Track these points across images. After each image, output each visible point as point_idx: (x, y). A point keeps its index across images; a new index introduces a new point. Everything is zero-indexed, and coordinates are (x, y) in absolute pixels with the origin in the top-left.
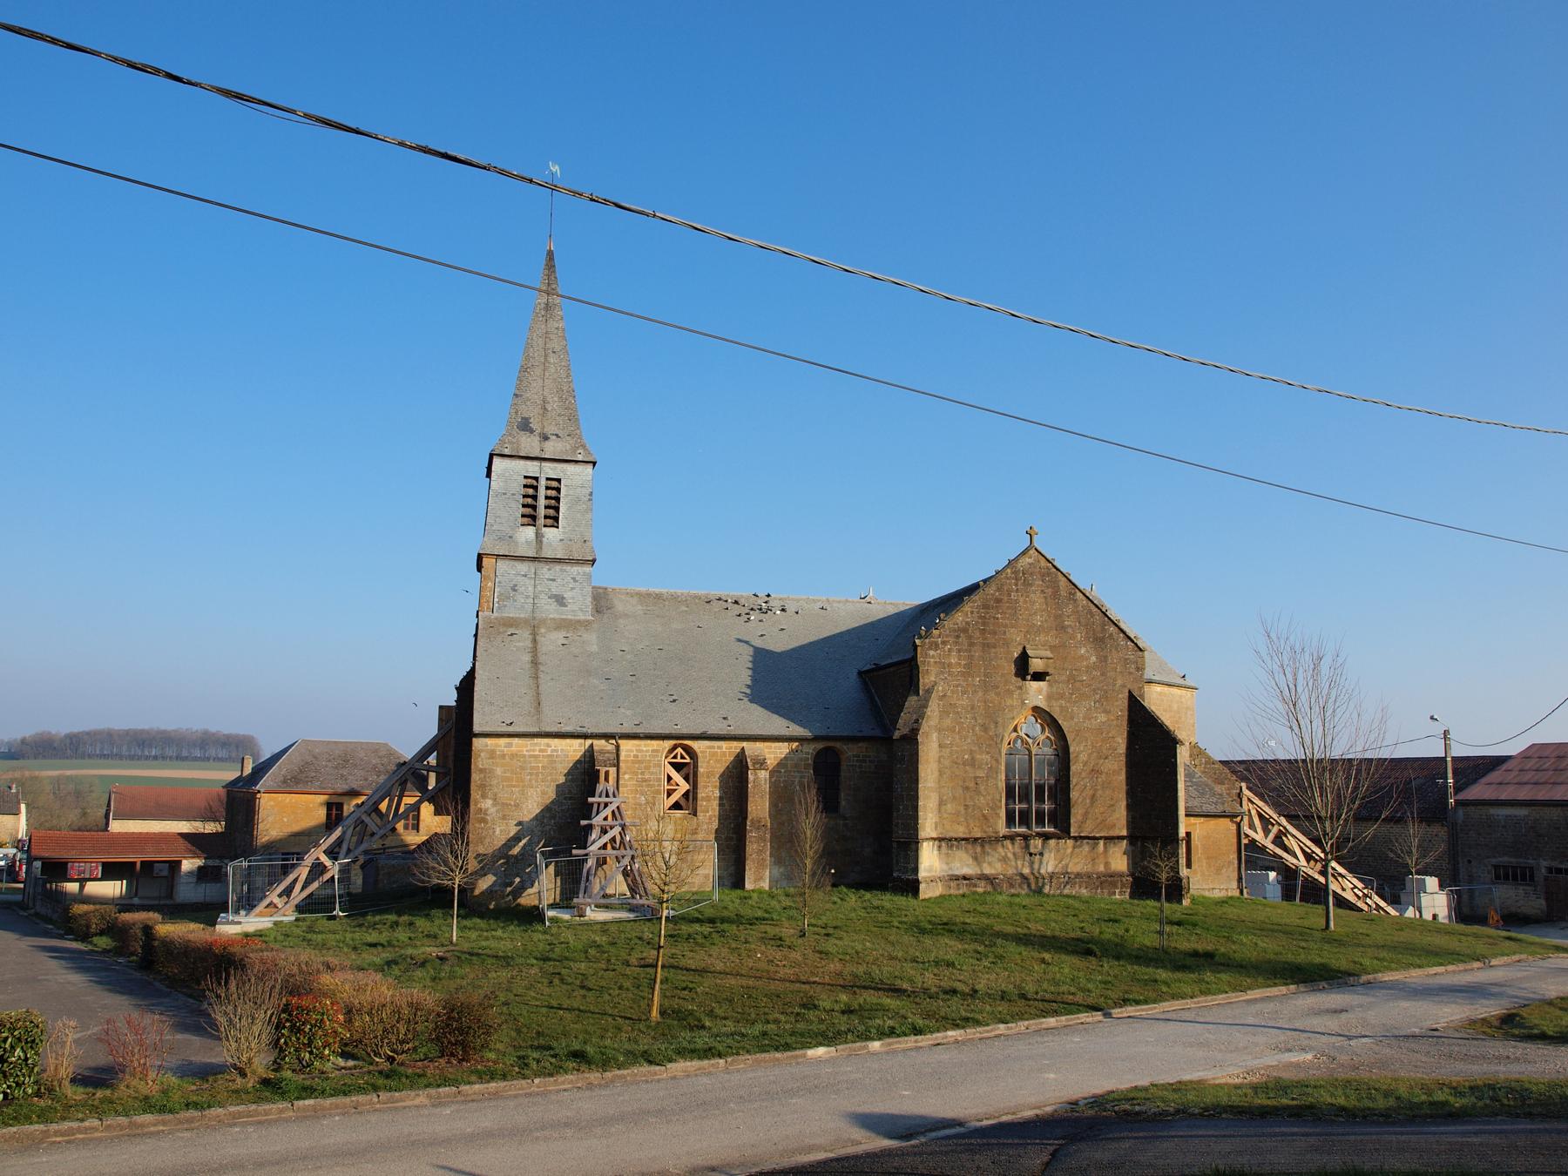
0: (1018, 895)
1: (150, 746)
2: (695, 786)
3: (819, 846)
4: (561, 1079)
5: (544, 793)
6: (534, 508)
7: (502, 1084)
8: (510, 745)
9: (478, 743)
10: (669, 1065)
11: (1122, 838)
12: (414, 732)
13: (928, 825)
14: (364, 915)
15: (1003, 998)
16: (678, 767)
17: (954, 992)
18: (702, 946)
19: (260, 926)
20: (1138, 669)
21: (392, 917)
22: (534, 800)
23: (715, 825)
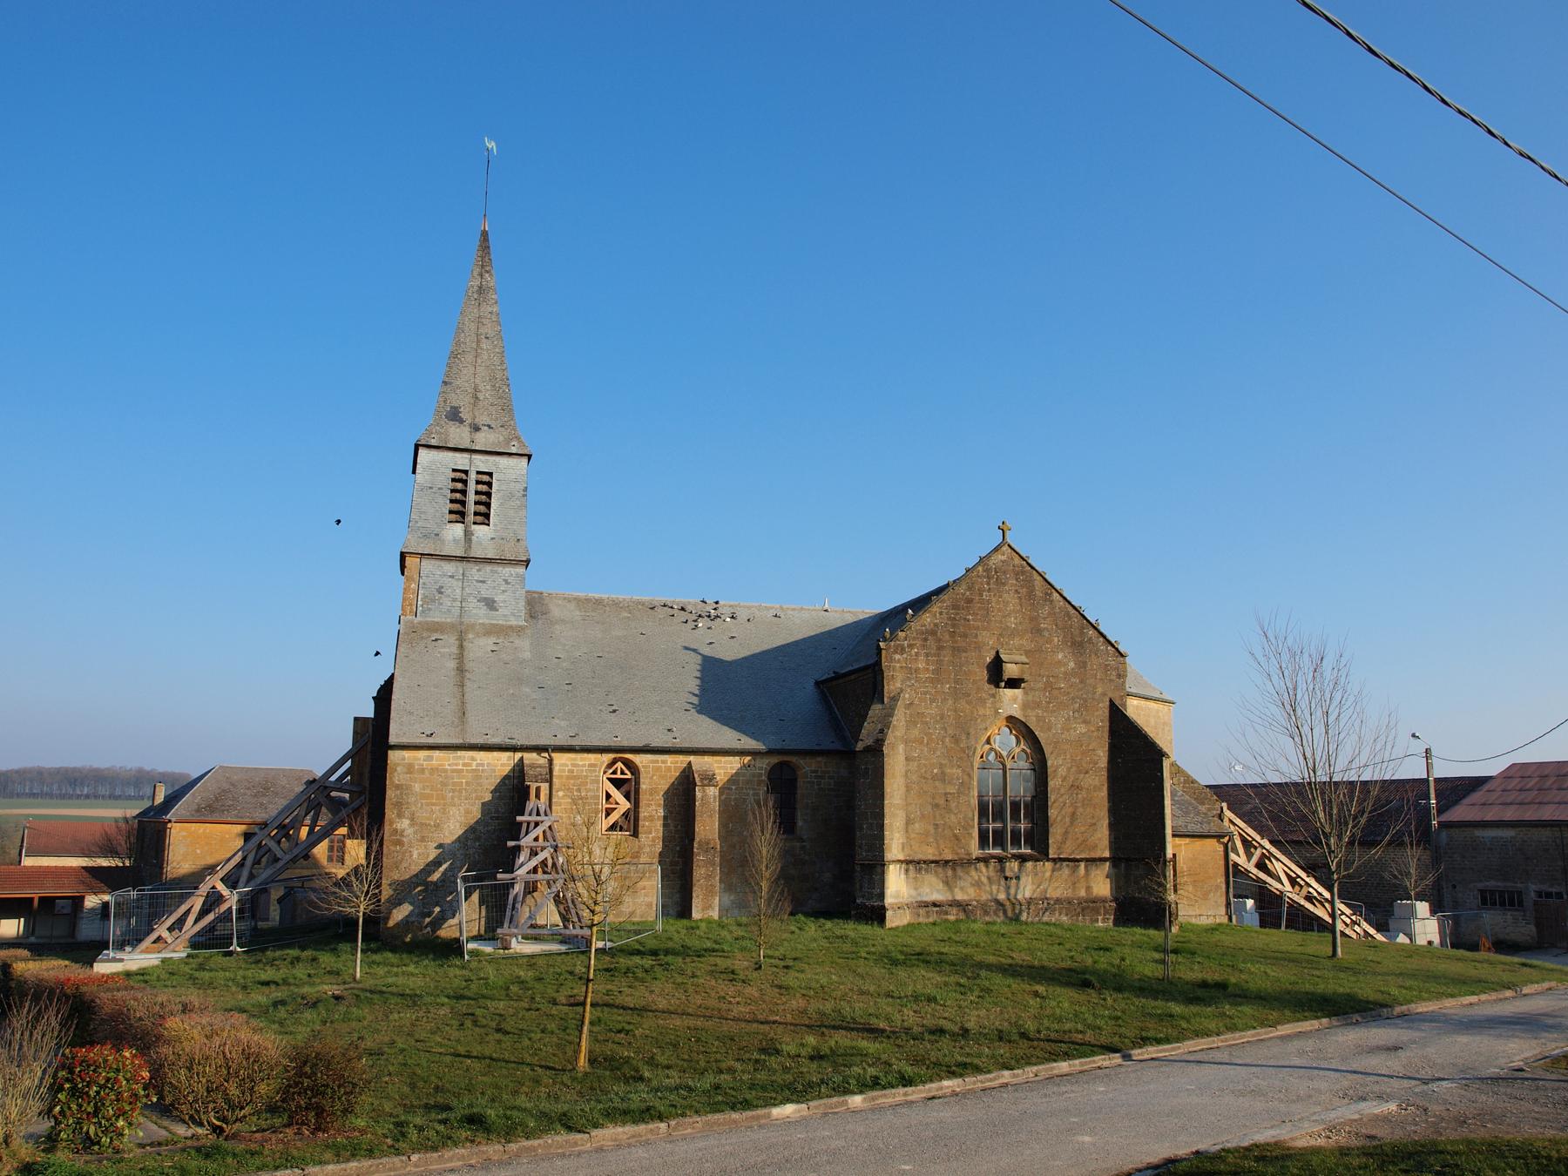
0: (994, 923)
1: (82, 784)
2: (636, 805)
3: (775, 867)
4: (448, 1154)
5: (467, 812)
6: (463, 503)
7: (366, 1163)
8: (430, 758)
9: (393, 756)
10: (594, 1132)
12: (325, 747)
13: (895, 845)
14: (263, 950)
15: (1001, 1039)
16: (618, 783)
18: (643, 981)
19: (145, 964)
20: (1119, 676)
21: (294, 952)
22: (455, 820)
23: (659, 847)
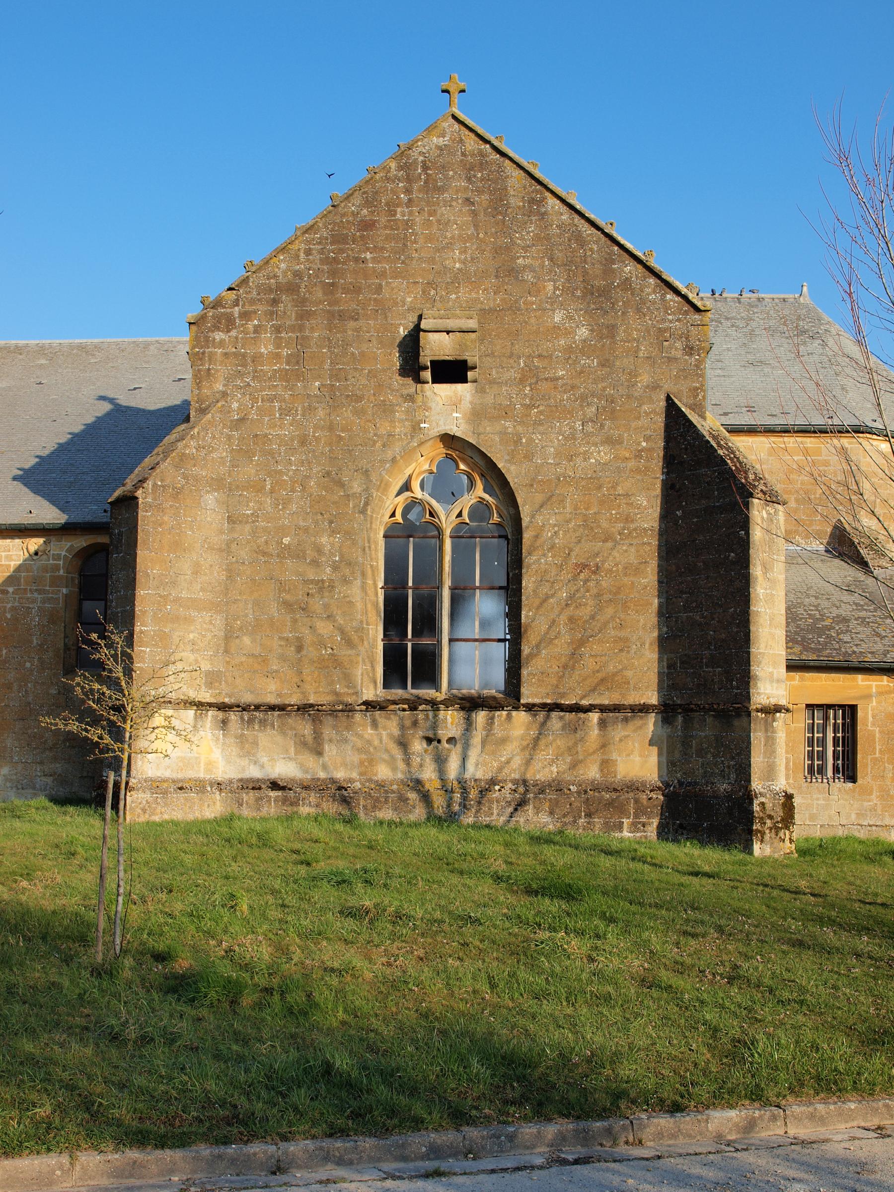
11: (643, 709)
17: (710, 1153)
20: (689, 350)
